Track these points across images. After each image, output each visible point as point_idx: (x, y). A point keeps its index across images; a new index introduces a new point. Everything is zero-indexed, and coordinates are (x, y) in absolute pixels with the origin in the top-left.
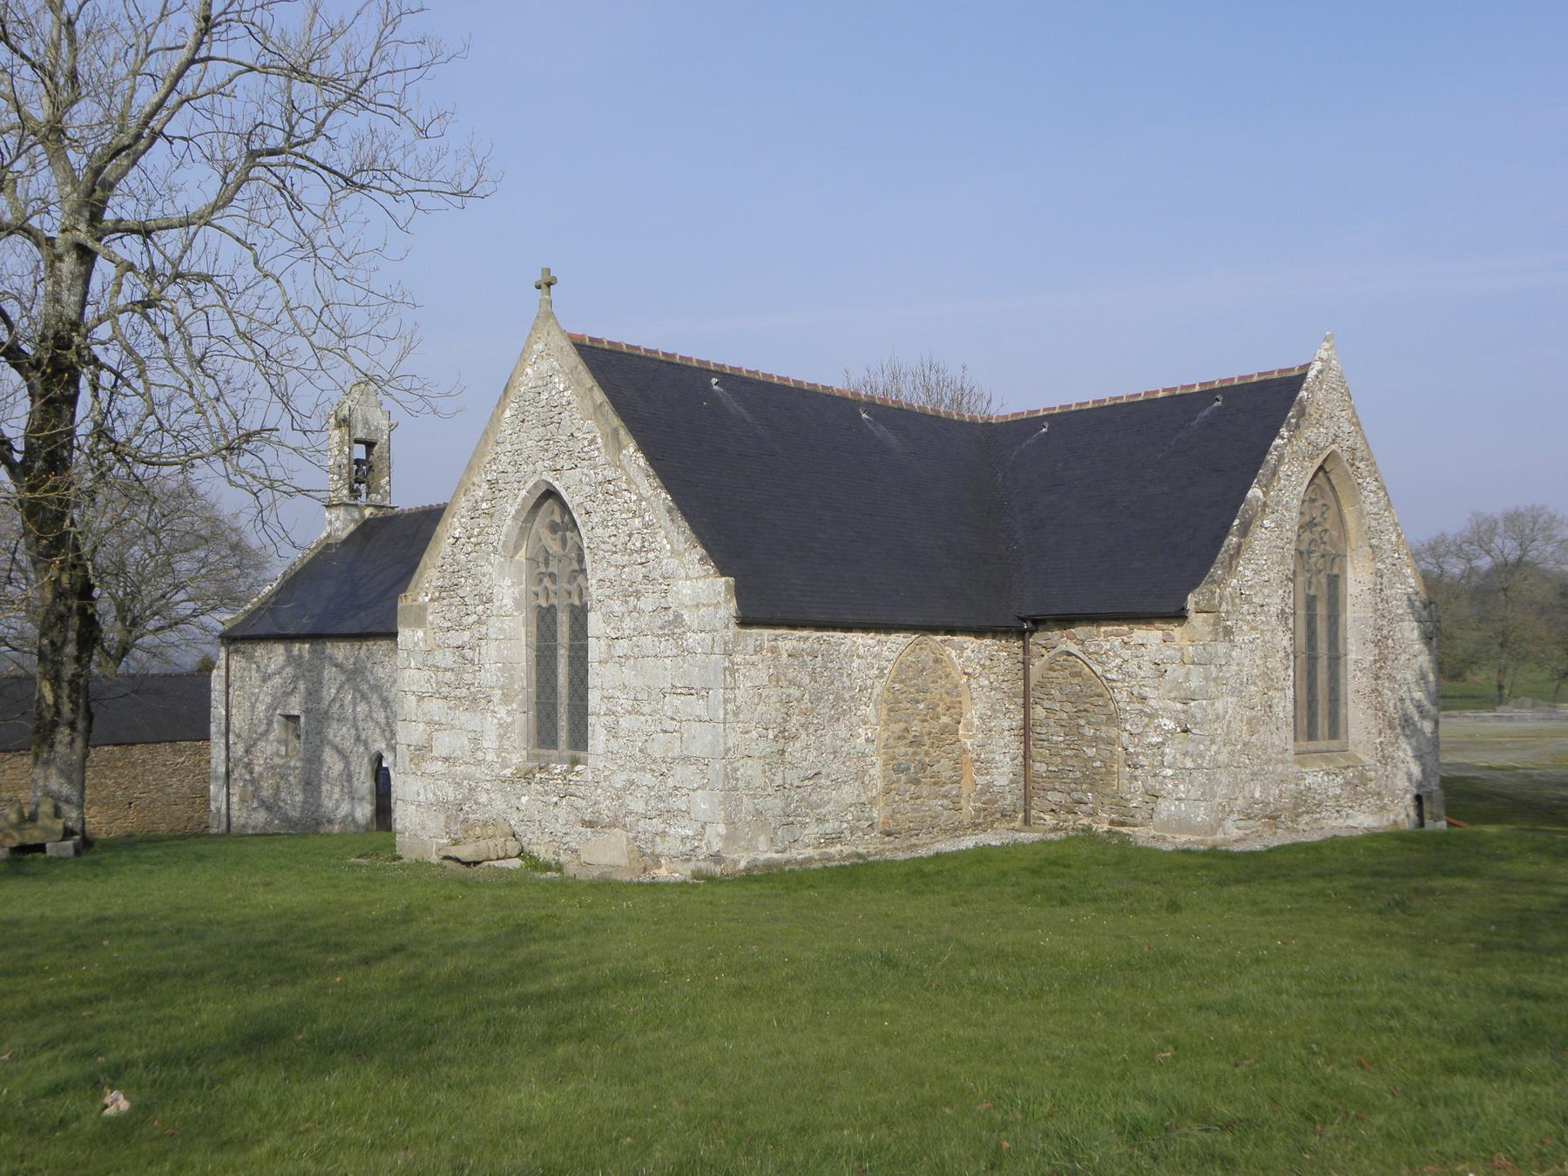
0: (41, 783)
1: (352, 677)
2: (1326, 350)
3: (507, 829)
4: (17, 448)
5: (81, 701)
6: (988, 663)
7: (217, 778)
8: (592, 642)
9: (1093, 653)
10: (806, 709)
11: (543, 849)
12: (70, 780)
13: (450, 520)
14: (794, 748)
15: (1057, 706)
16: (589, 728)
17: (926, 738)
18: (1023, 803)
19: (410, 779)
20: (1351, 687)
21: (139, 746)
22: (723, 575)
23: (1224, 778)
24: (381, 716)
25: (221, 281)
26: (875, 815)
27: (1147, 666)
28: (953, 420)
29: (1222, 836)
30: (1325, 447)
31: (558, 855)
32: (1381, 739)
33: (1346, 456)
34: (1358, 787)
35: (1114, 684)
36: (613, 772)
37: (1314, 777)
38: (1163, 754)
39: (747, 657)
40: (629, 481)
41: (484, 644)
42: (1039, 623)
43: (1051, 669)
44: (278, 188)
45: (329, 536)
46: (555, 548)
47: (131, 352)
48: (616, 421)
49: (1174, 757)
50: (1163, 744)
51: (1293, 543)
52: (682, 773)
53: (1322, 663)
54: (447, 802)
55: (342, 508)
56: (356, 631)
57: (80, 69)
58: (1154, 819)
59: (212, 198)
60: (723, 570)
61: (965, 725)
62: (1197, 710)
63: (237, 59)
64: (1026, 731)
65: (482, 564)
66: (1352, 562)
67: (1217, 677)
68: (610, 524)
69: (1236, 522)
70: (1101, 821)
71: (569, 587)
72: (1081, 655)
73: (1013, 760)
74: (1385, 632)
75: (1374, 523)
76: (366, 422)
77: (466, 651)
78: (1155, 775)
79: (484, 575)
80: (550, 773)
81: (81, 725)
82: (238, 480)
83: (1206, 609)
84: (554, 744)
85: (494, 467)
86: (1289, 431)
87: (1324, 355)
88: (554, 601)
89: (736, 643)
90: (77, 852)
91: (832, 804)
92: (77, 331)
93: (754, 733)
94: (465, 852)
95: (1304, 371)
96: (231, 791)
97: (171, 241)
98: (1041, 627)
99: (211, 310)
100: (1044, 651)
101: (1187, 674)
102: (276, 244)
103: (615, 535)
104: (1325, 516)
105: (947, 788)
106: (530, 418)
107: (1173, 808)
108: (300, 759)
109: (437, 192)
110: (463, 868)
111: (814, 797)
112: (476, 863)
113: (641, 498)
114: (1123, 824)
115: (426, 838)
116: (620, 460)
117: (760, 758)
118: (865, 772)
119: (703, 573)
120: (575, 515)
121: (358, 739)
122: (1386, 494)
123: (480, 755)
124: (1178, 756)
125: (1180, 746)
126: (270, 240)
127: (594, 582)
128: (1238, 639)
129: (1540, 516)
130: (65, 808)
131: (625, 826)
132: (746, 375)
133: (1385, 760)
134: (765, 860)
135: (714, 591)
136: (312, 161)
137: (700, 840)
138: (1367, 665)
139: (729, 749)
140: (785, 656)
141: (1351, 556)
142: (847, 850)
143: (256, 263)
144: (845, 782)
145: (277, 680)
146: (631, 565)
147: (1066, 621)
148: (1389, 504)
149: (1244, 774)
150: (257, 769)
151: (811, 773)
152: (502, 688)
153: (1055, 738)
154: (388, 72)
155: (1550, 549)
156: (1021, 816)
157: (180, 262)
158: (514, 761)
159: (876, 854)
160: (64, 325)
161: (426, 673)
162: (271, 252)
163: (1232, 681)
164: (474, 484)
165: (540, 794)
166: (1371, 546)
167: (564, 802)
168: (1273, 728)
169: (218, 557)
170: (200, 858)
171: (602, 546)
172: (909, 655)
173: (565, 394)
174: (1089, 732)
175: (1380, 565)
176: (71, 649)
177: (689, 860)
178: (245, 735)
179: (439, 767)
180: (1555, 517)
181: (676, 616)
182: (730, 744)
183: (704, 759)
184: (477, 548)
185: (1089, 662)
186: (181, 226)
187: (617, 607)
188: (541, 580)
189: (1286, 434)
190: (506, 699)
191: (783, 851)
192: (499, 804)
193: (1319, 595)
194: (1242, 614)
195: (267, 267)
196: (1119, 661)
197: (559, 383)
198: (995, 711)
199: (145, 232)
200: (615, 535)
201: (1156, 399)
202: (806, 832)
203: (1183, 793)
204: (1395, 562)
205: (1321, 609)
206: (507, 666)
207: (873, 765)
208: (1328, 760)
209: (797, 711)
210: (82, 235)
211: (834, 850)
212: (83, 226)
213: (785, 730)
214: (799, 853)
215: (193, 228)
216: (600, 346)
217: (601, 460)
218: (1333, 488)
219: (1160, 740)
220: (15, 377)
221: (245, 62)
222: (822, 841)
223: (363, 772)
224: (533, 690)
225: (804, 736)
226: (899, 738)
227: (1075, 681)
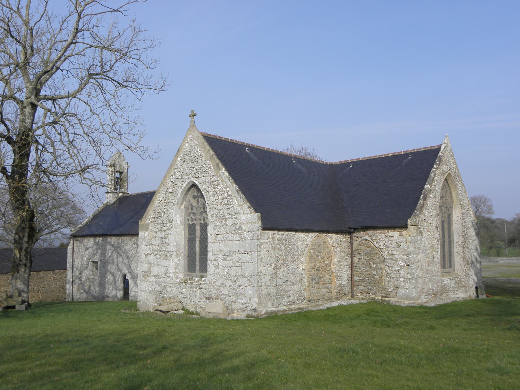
1: (116, 249)
2: (446, 140)
3: (178, 300)
4: (8, 171)
5: (28, 256)
6: (340, 243)
7: (69, 283)
8: (209, 236)
9: (375, 239)
10: (283, 258)
11: (191, 307)
12: (24, 284)
13: (158, 195)
14: (280, 272)
15: (362, 257)
16: (208, 265)
17: (321, 268)
18: (351, 290)
19: (143, 283)
20: (455, 251)
21: (42, 272)
22: (256, 213)
23: (421, 281)
24: (126, 261)
25: (79, 116)
26: (305, 295)
27: (394, 244)
28: (320, 163)
29: (421, 301)
30: (447, 172)
31: (197, 309)
32: (465, 268)
33: (453, 175)
34: (459, 284)
35: (382, 250)
36: (217, 280)
37: (447, 281)
38: (400, 274)
39: (265, 241)
40: (223, 181)
41: (170, 237)
42: (356, 229)
43: (360, 245)
44: (98, 86)
45: (107, 202)
46: (195, 204)
47: (49, 138)
48: (218, 161)
49: (404, 274)
50: (400, 270)
51: (439, 203)
52: (242, 280)
53: (447, 243)
54: (156, 291)
55: (112, 193)
56: (118, 233)
57: (34, 46)
58: (397, 295)
59: (77, 88)
60: (256, 211)
61: (333, 264)
62: (412, 258)
63: (87, 43)
64: (352, 266)
65: (169, 209)
66: (455, 210)
67: (418, 247)
68: (216, 195)
69: (422, 196)
70: (378, 296)
71: (200, 217)
72: (371, 240)
73: (348, 275)
74: (465, 233)
75: (461, 197)
76: (120, 166)
77: (163, 239)
78: (397, 281)
79: (170, 213)
80: (193, 281)
81: (28, 264)
82: (84, 182)
83: (414, 225)
84: (194, 271)
85: (174, 177)
86: (437, 166)
87: (446, 142)
88: (194, 222)
89: (261, 236)
90: (26, 309)
91: (292, 291)
92: (31, 132)
93: (267, 267)
94: (164, 308)
95: (439, 147)
96: (74, 287)
97: (62, 103)
98: (356, 231)
99: (75, 126)
100: (357, 239)
101: (408, 246)
102: (98, 103)
103: (217, 199)
104: (446, 194)
105: (327, 285)
106: (187, 160)
107: (404, 292)
108: (98, 276)
109: (150, 88)
110: (163, 314)
111: (286, 289)
112: (168, 312)
113: (227, 187)
114: (386, 297)
115: (148, 303)
116: (219, 174)
117: (269, 275)
118: (302, 280)
119: (250, 212)
120: (203, 193)
121: (118, 269)
122: (464, 188)
123: (168, 275)
124: (405, 274)
125: (406, 271)
126: (95, 103)
127: (210, 215)
128: (424, 235)
129: (482, 198)
130: (22, 293)
131: (221, 299)
132: (256, 147)
133: (467, 275)
134: (270, 311)
135: (254, 218)
136: (110, 78)
137: (249, 304)
138: (460, 243)
139: (259, 272)
140: (277, 240)
141: (454, 208)
142: (297, 307)
143: (91, 110)
144: (296, 283)
145: (91, 250)
146: (223, 209)
147: (365, 229)
148: (465, 191)
149: (427, 280)
150: (83, 279)
151: (285, 280)
152: (176, 252)
153: (362, 268)
154: (134, 50)
155: (485, 209)
156: (350, 294)
157: (65, 110)
158: (180, 277)
159: (306, 308)
160: (26, 129)
161: (149, 247)
162: (96, 107)
163: (422, 249)
164: (166, 183)
165: (190, 288)
166: (461, 204)
167: (199, 290)
168: (435, 264)
169: (67, 210)
170: (71, 311)
171: (213, 203)
172: (315, 240)
173: (200, 152)
174: (374, 266)
175: (463, 211)
176: (26, 239)
177: (244, 311)
178: (79, 268)
179: (153, 279)
180: (486, 198)
181: (240, 227)
182: (259, 271)
183: (250, 276)
184: (167, 204)
185: (373, 243)
186: (66, 98)
187: (218, 223)
188: (190, 215)
189: (436, 167)
190: (177, 255)
191: (276, 307)
192: (175, 291)
193: (445, 220)
194: (425, 226)
195: (95, 112)
196: (384, 242)
197: (198, 148)
198: (342, 259)
199: (54, 100)
200: (217, 199)
201: (389, 156)
202: (284, 301)
203: (407, 286)
204: (468, 210)
205: (446, 225)
206: (178, 244)
207: (305, 277)
208: (450, 275)
209: (280, 259)
210: (33, 99)
211: (292, 307)
212: (33, 97)
213: (277, 266)
214: (282, 308)
215: (70, 98)
216: (210, 136)
217: (212, 174)
218: (449, 185)
219: (399, 268)
220: (10, 147)
221: (89, 44)
222: (289, 304)
224: (186, 252)
225: (283, 268)
226: (313, 268)
227: (369, 249)
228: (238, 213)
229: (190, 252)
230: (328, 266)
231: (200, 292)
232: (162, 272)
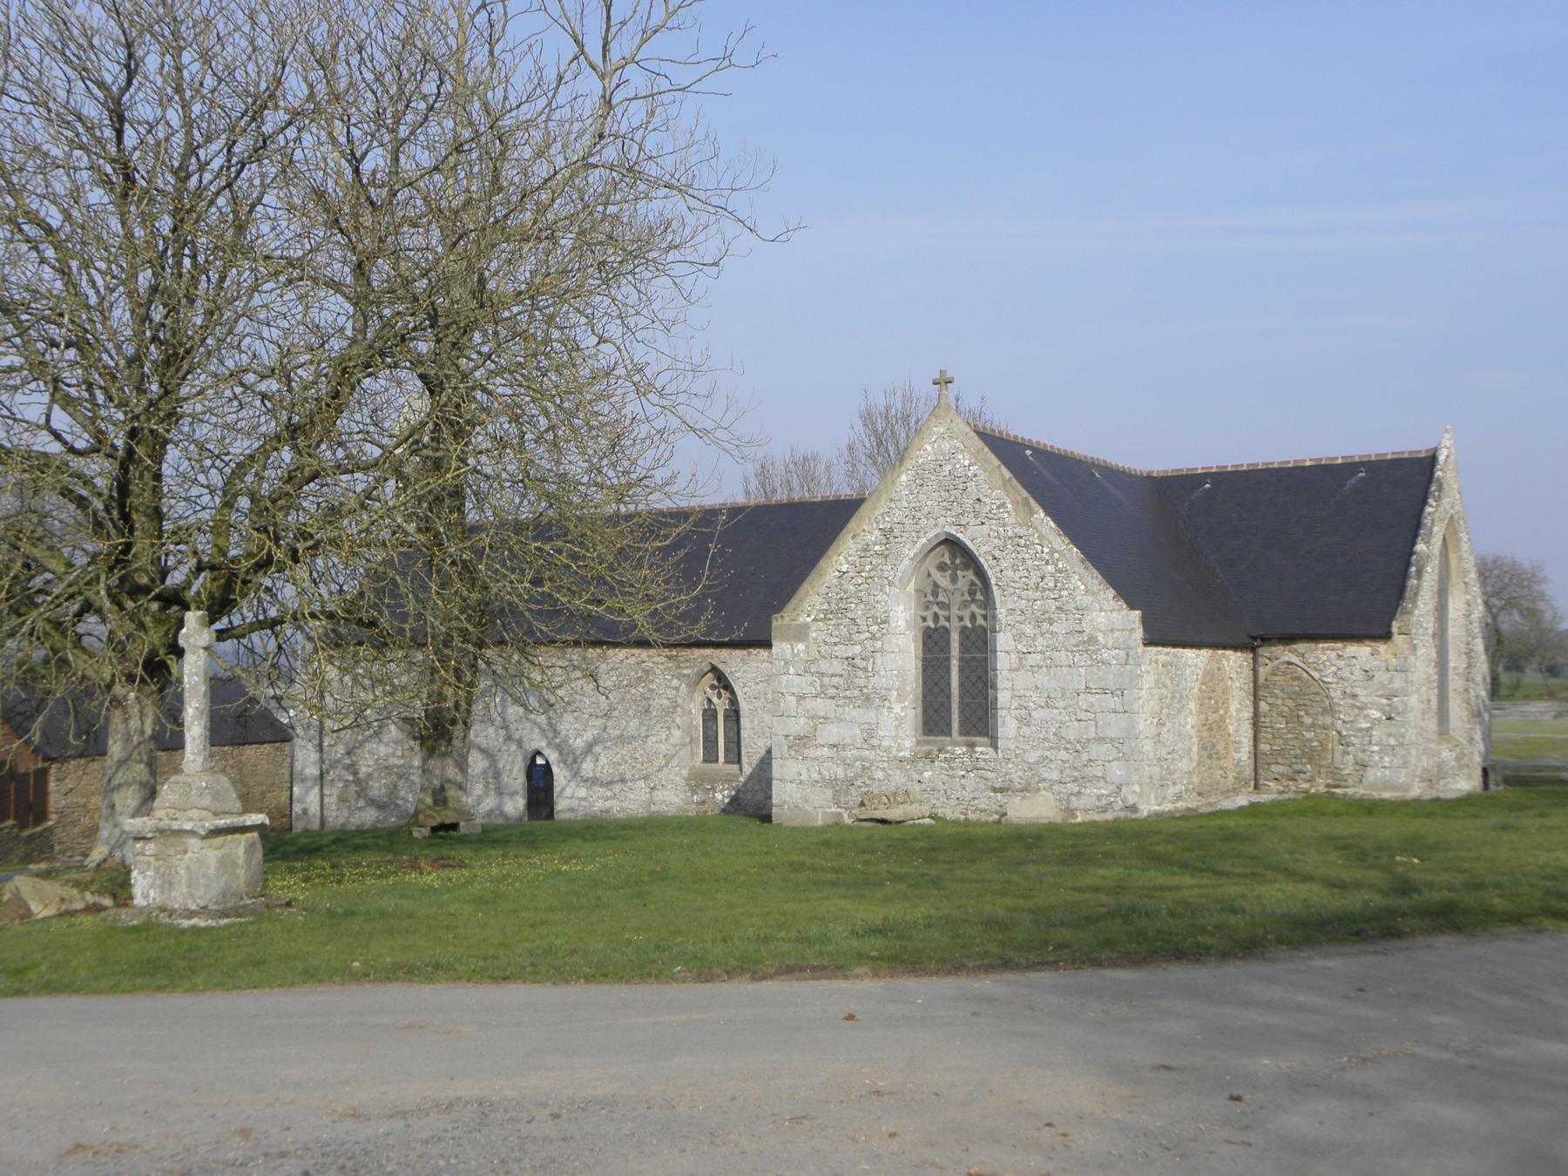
0: (437, 772)
13: (835, 558)
15: (1280, 702)
27: (1358, 674)
38: (1371, 736)
40: (1041, 537)
42: (1266, 640)
48: (1025, 494)
50: (1371, 728)
52: (1096, 750)
60: (1132, 607)
71: (961, 613)
96: (325, 792)
113: (1053, 550)
114: (1336, 786)
121: (509, 738)
127: (1003, 610)
147: (1288, 639)
161: (809, 678)
187: (1029, 630)
190: (900, 698)
196: (1333, 669)
217: (1010, 520)
223: (516, 770)
224: (920, 691)
227: (1296, 683)
228: (1087, 608)
229: (930, 690)
230: (1223, 719)
231: (976, 776)
232: (855, 735)
